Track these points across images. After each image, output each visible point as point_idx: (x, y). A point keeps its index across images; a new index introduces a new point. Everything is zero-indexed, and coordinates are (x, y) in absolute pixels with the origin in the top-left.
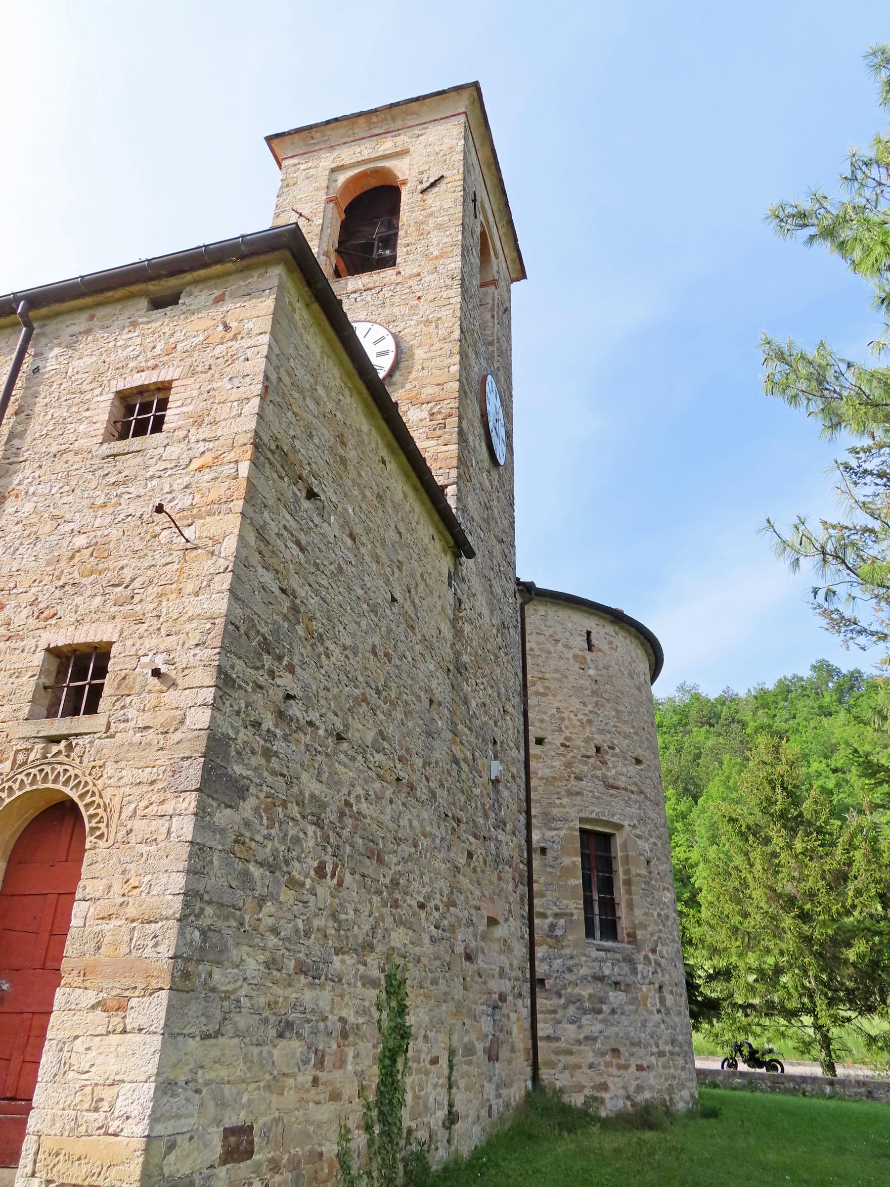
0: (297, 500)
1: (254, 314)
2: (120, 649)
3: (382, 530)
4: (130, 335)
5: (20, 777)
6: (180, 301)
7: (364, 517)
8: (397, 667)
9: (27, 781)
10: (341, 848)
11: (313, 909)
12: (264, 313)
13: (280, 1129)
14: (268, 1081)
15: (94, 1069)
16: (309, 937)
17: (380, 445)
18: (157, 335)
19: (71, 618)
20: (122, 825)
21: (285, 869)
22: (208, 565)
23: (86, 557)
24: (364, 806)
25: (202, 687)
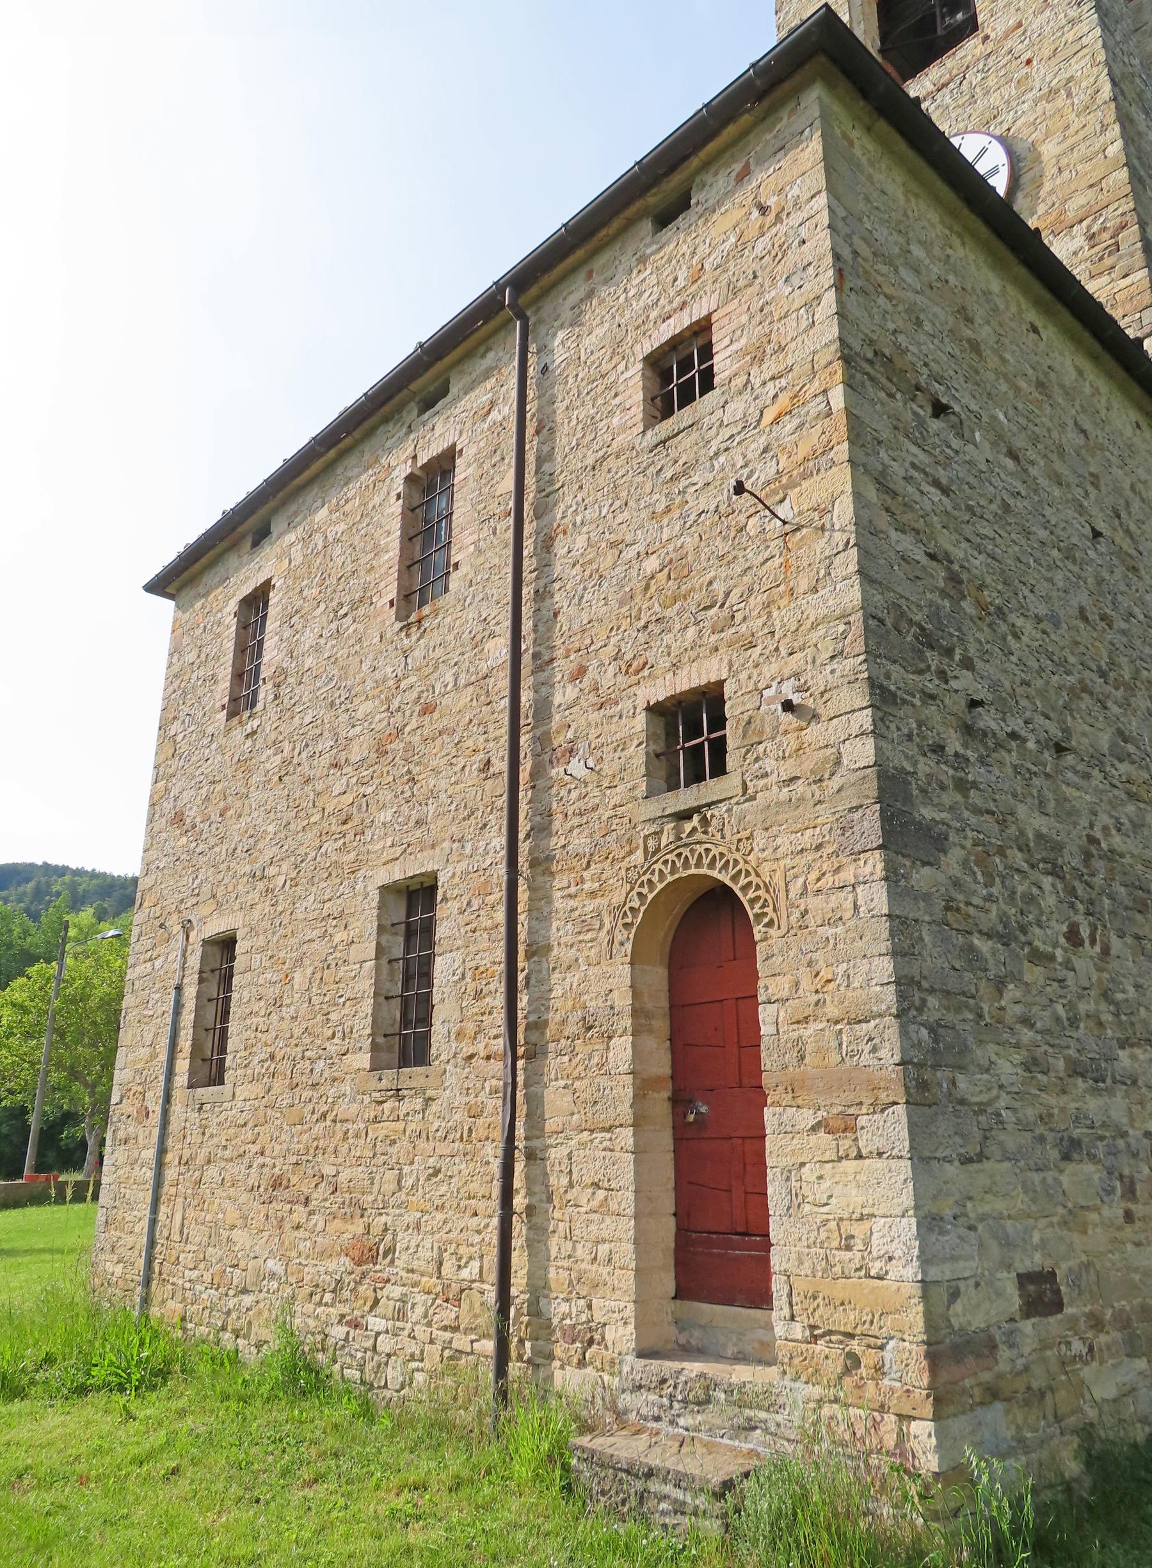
0: (921, 423)
1: (796, 172)
2: (734, 687)
3: (1055, 435)
4: (642, 276)
5: (657, 866)
6: (693, 202)
7: (1023, 422)
8: (1124, 632)
9: (667, 871)
10: (1097, 903)
11: (1074, 988)
12: (810, 165)
13: (1093, 1277)
14: (1063, 1216)
15: (833, 1201)
16: (1078, 1027)
17: (1024, 306)
18: (674, 261)
19: (664, 663)
20: (792, 905)
21: (1023, 938)
22: (821, 546)
23: (664, 582)
24: (1117, 840)
25: (854, 711)
